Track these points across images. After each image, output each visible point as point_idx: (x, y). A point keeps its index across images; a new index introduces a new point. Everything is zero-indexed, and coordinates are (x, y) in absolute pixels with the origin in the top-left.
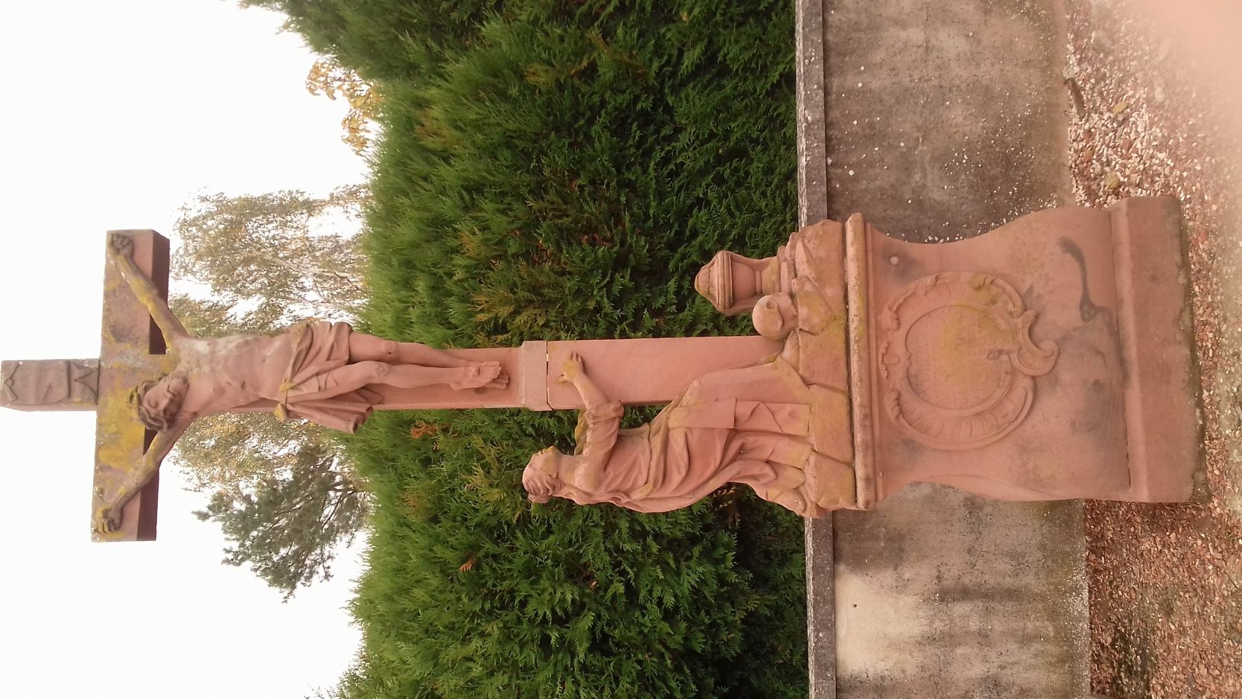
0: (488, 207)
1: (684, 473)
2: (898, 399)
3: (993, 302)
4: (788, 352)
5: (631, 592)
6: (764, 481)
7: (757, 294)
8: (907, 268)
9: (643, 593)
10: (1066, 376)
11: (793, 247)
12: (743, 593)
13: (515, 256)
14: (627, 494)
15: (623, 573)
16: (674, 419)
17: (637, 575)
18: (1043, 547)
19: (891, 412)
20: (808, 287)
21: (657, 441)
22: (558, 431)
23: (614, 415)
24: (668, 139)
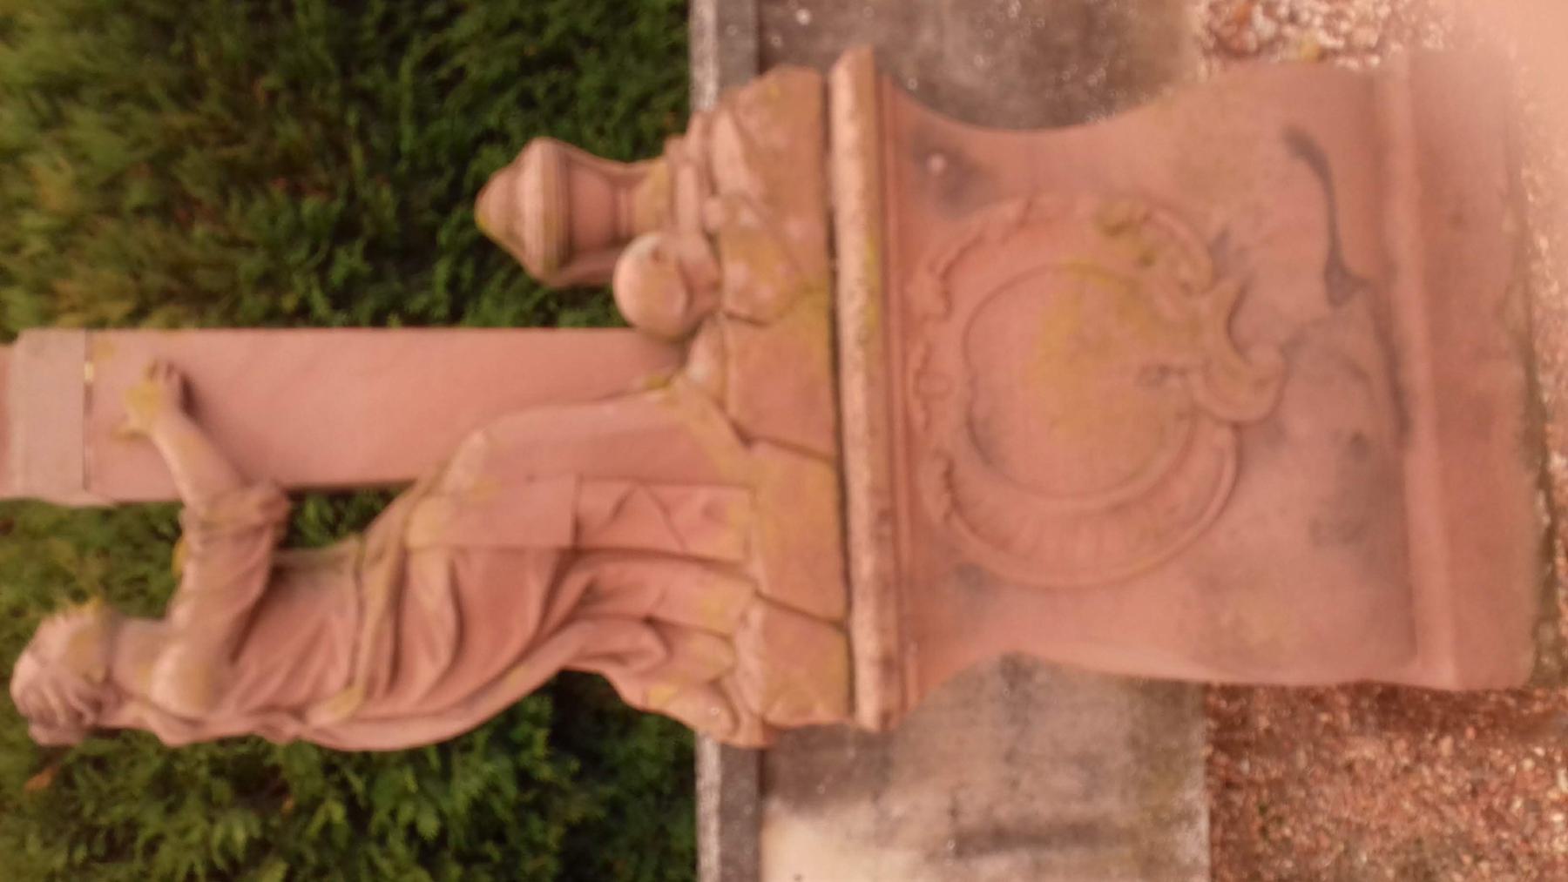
0: (86, 123)
1: (444, 655)
2: (949, 474)
3: (1146, 261)
4: (701, 364)
5: (359, 814)
6: (643, 665)
7: (618, 240)
8: (963, 183)
9: (380, 817)
10: (1300, 424)
11: (708, 131)
12: (562, 793)
13: (140, 211)
14: (298, 713)
15: (344, 785)
16: (419, 525)
17: (370, 784)
18: (1134, 742)
19: (934, 504)
20: (747, 217)
21: (378, 582)
22: (131, 553)
23: (256, 518)
24: (439, 25)
